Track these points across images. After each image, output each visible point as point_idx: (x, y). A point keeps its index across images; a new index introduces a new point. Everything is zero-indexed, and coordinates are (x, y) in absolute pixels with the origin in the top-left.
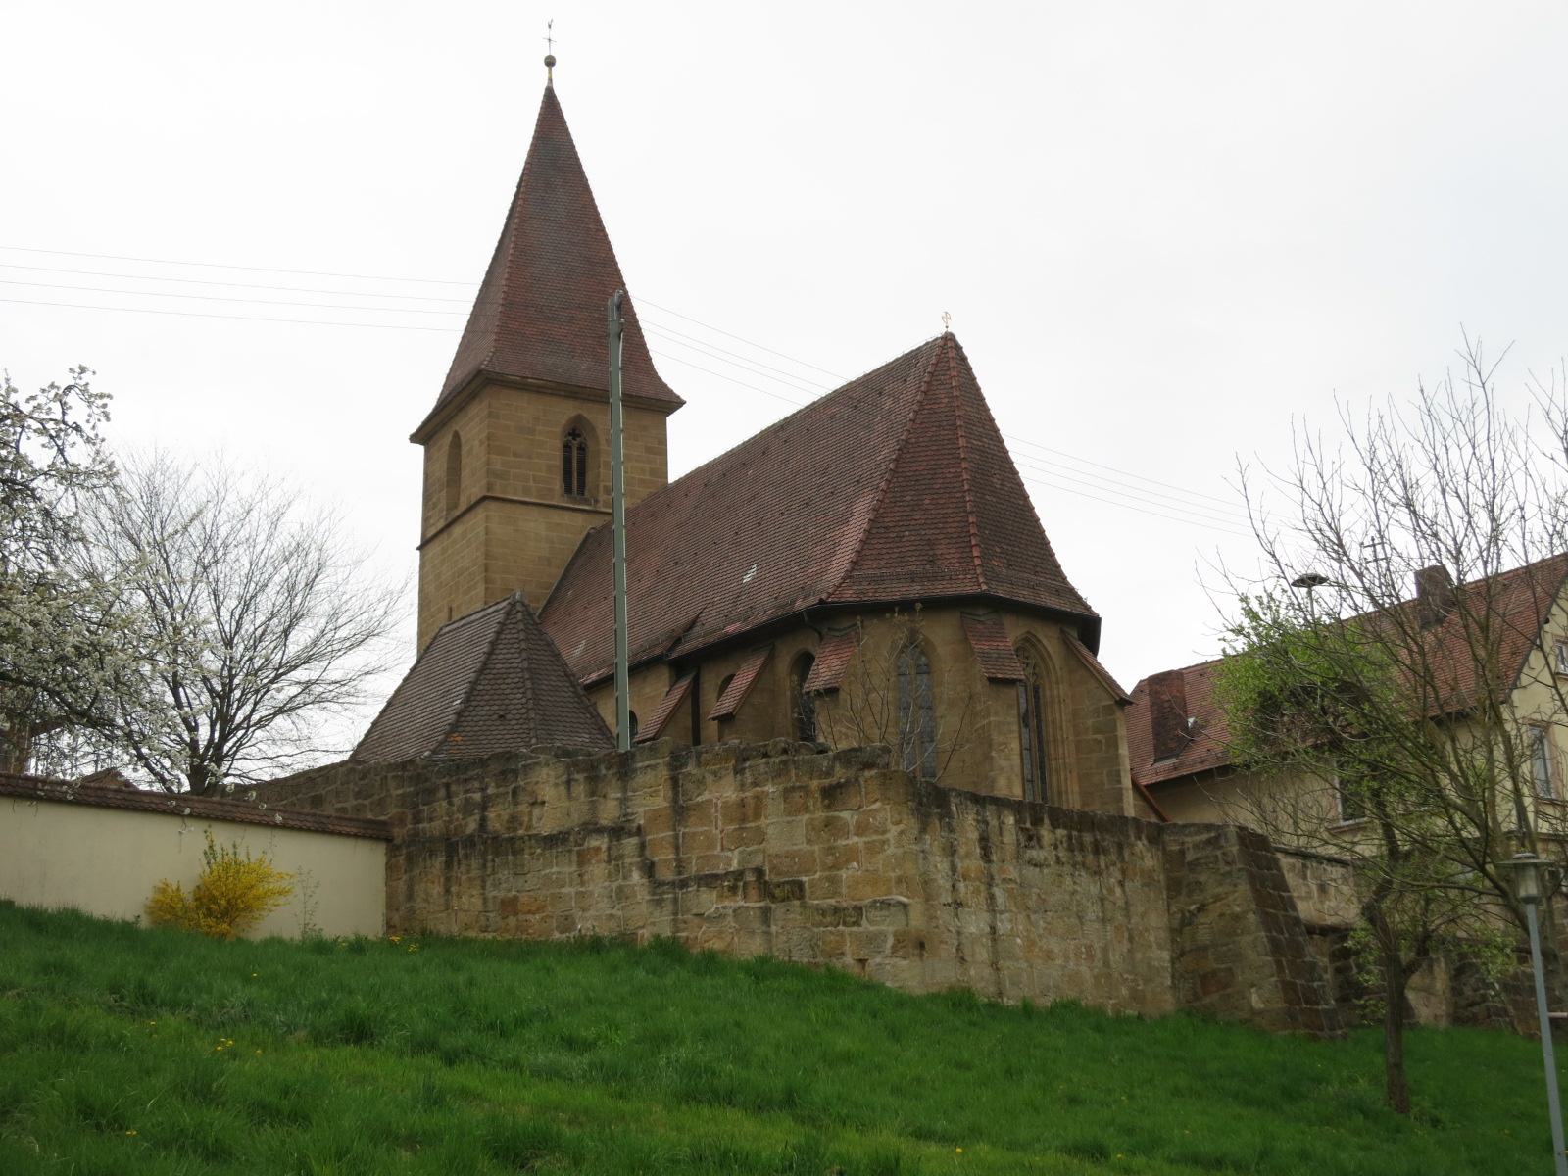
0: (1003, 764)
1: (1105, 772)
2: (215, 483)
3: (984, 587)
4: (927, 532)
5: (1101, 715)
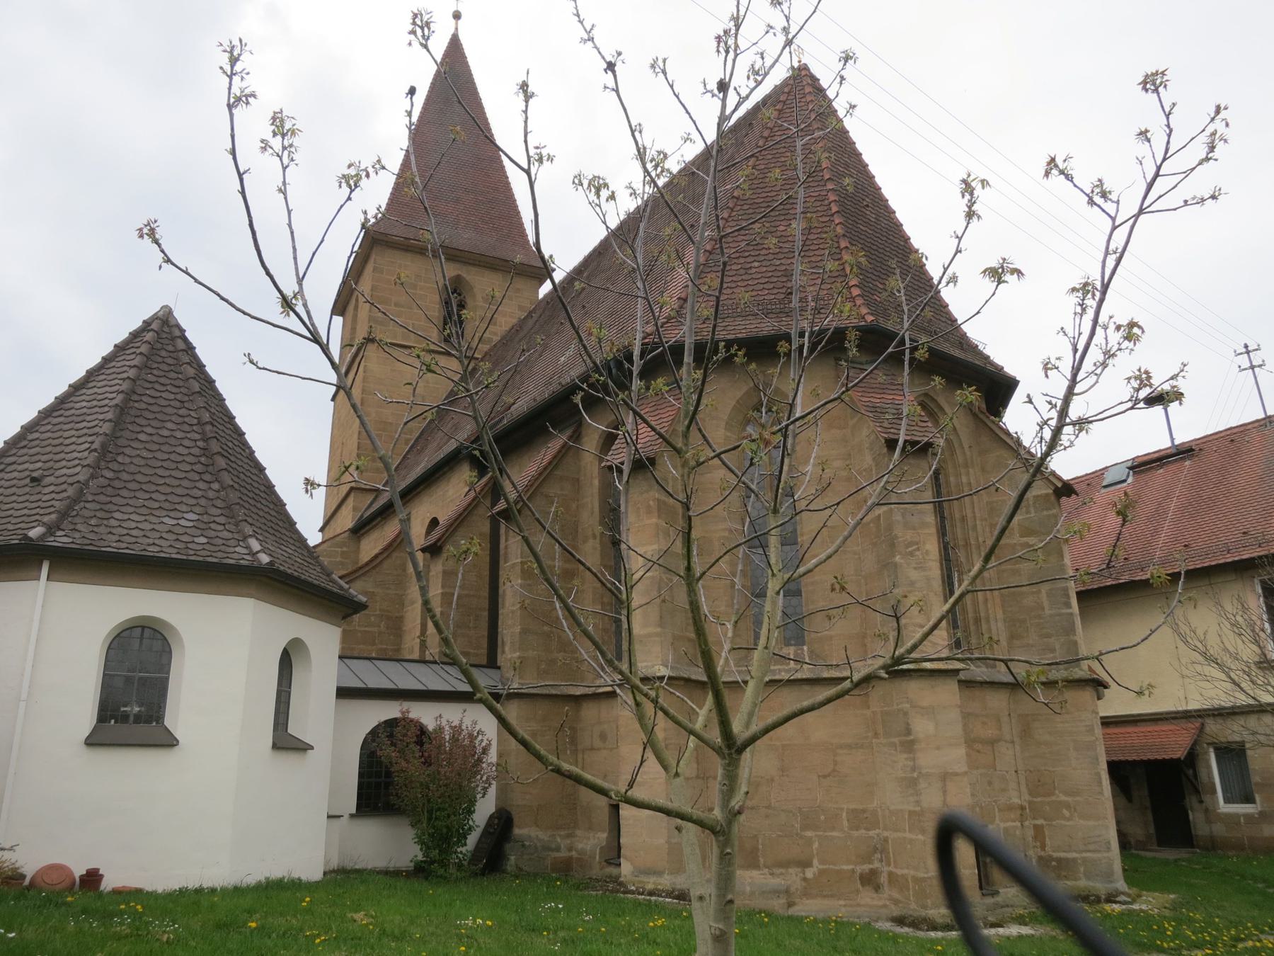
0: (914, 575)
3: (870, 318)
4: (783, 261)
5: (1032, 510)
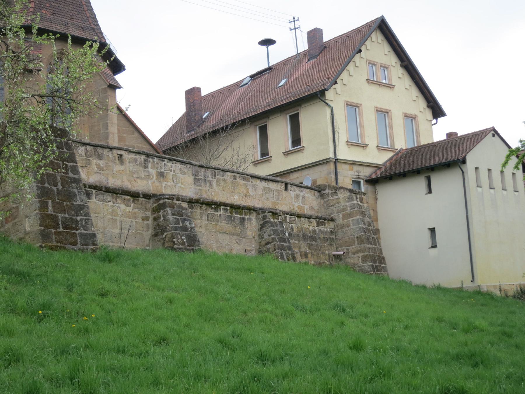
1: (101, 124)
2: (75, 112)
